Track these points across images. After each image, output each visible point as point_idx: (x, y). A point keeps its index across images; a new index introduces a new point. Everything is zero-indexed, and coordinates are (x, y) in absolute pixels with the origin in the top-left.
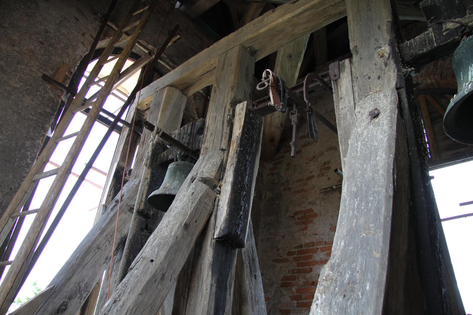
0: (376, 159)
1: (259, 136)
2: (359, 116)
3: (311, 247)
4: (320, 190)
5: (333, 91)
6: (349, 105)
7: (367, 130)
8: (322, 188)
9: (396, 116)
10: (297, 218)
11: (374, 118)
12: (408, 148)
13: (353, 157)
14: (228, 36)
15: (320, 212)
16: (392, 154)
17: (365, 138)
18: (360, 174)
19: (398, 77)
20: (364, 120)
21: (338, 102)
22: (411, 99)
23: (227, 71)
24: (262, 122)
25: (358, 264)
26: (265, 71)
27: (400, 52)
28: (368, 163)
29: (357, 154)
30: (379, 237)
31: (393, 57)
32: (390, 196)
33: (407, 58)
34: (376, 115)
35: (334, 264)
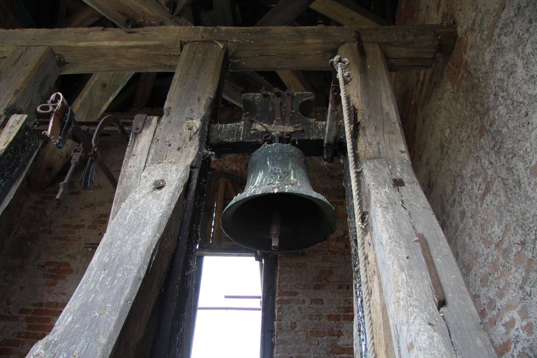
0: (141, 233)
1: (27, 161)
2: (143, 181)
3: (53, 309)
4: (86, 244)
5: (129, 145)
6: (138, 165)
7: (145, 199)
8: (88, 242)
9: (179, 195)
10: (47, 269)
11: (157, 189)
12: (180, 230)
13: (118, 224)
14: (39, 30)
15: (78, 269)
16: (159, 234)
17: (139, 207)
18: (118, 245)
19: (196, 156)
20: (146, 188)
21: (129, 158)
22: (202, 182)
23: (18, 70)
24: (38, 146)
25: (78, 346)
26: (56, 94)
27: (208, 132)
28: (131, 235)
29: (125, 221)
30: (112, 320)
31: (200, 134)
32: (141, 278)
33: (212, 140)
34: (160, 186)
35: (51, 341)
